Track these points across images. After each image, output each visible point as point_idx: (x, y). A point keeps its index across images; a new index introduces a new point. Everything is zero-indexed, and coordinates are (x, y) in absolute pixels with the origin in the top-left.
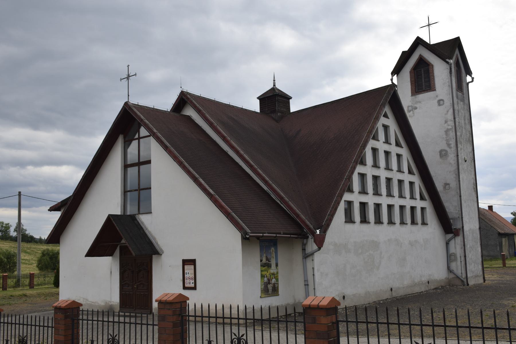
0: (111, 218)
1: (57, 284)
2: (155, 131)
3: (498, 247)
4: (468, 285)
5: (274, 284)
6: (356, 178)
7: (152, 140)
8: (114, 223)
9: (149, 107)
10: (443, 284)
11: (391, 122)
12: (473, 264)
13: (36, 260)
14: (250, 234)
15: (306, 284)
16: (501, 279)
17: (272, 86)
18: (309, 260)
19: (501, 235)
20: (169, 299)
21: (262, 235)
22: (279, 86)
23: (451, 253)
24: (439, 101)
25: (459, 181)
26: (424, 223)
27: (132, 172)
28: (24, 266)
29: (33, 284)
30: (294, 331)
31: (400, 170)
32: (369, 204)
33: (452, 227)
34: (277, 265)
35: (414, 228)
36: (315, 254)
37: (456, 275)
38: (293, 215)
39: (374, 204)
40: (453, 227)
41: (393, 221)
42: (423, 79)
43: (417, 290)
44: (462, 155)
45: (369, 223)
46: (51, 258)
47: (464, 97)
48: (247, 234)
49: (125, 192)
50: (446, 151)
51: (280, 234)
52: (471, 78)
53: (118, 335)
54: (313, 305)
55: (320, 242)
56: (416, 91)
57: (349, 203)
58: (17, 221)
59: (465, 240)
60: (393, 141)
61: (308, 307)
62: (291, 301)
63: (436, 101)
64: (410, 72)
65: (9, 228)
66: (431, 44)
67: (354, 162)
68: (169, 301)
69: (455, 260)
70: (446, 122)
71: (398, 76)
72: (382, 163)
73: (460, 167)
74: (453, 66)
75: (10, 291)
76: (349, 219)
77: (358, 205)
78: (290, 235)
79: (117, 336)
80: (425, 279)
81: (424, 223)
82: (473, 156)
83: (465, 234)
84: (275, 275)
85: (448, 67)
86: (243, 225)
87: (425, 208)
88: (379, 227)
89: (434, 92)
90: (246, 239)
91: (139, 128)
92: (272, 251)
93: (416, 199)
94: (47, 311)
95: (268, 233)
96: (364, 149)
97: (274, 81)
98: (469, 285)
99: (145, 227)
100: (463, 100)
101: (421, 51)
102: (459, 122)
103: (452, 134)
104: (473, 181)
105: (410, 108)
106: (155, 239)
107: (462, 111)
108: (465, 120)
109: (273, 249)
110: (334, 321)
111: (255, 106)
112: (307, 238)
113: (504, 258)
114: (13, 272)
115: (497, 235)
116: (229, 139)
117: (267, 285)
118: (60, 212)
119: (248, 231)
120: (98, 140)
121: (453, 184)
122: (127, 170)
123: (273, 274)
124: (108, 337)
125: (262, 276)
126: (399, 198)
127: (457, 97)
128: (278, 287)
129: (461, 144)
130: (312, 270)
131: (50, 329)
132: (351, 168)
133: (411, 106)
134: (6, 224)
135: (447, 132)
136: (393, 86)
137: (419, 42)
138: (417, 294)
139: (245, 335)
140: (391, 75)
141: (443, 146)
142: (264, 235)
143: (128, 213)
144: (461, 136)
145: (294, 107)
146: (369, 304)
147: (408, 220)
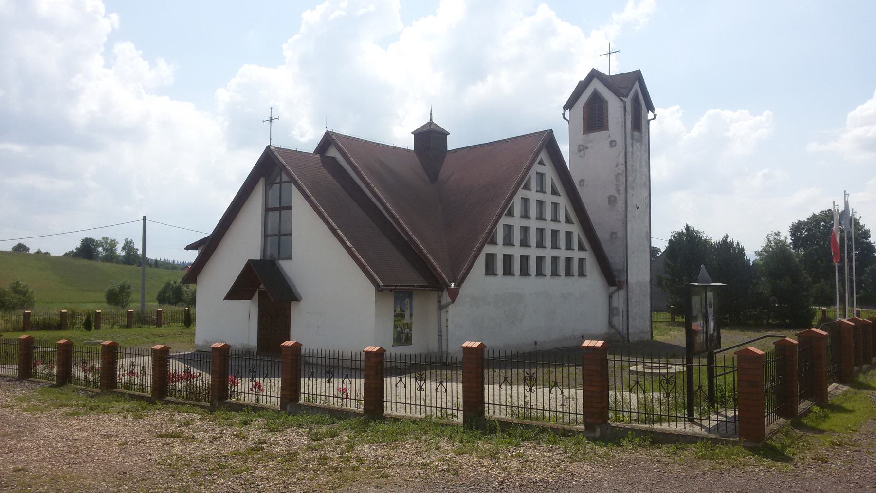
17: (429, 121)
18: (443, 311)
23: (615, 307)
24: (611, 142)
26: (582, 274)
33: (616, 279)
34: (411, 316)
36: (450, 306)
37: (617, 330)
44: (632, 202)
50: (615, 197)
52: (653, 114)
55: (454, 294)
60: (548, 189)
63: (608, 142)
70: (617, 166)
71: (571, 110)
76: (490, 270)
77: (502, 257)
82: (648, 202)
88: (525, 280)
90: (379, 289)
92: (406, 302)
97: (431, 114)
101: (596, 84)
103: (622, 179)
105: (581, 148)
109: (407, 300)
111: (409, 143)
117: (400, 334)
118: (197, 251)
123: (407, 324)
125: (395, 326)
126: (521, 248)
127: (632, 138)
128: (411, 337)
130: (446, 321)
133: (583, 145)
134: (112, 241)
135: (617, 176)
140: (563, 110)
141: (612, 191)
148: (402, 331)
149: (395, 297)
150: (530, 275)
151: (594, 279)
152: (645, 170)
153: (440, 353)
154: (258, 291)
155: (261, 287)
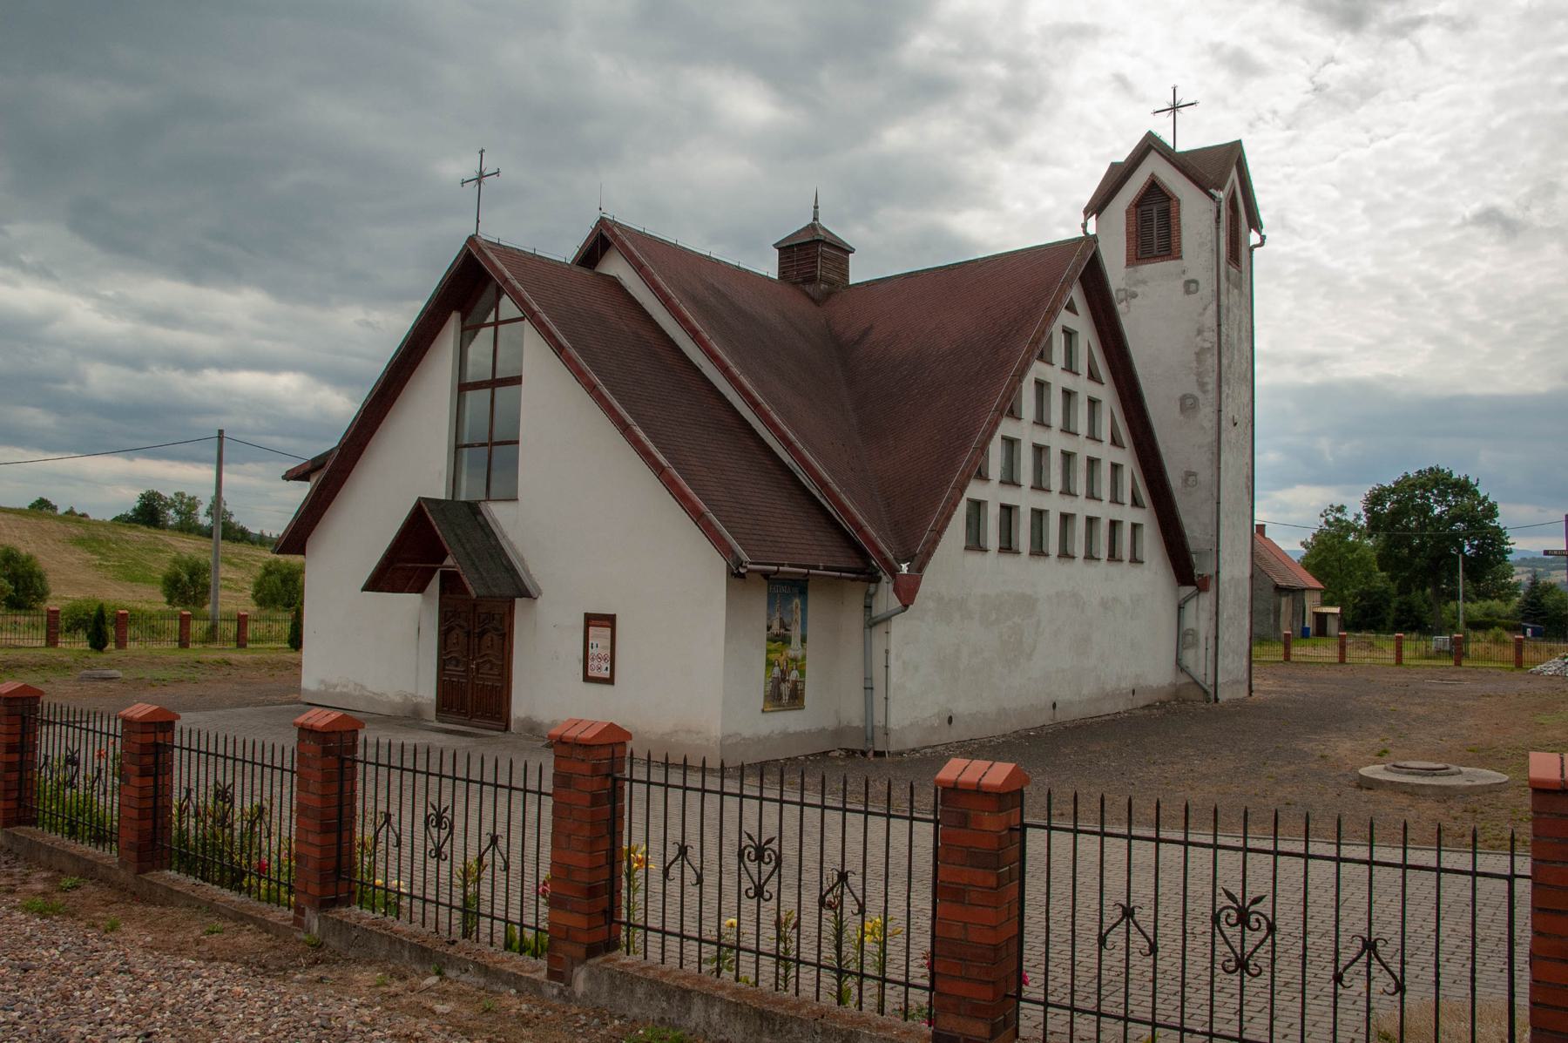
0: (424, 505)
1: (296, 641)
2: (536, 307)
3: (1272, 616)
4: (1216, 700)
5: (795, 683)
6: (996, 450)
7: (528, 328)
8: (431, 518)
9: (524, 252)
10: (1163, 697)
11: (1081, 323)
12: (1231, 656)
13: (249, 582)
14: (749, 566)
15: (869, 685)
16: (1284, 689)
17: (810, 220)
18: (878, 632)
19: (1279, 590)
20: (582, 736)
21: (776, 568)
22: (827, 223)
24: (1188, 283)
25: (1219, 468)
26: (1135, 560)
27: (477, 401)
28: (226, 593)
29: (245, 638)
30: (841, 795)
31: (1093, 436)
32: (1021, 509)
34: (804, 640)
35: (1114, 569)
36: (893, 618)
38: (847, 526)
39: (1033, 510)
40: (1197, 572)
41: (1069, 552)
42: (1155, 229)
43: (1108, 708)
44: (1229, 411)
45: (1018, 553)
46: (284, 581)
47: (1241, 278)
48: (741, 565)
49: (458, 447)
50: (1195, 399)
51: (816, 568)
53: (1270, 897)
54: (965, 783)
55: (907, 594)
56: (1136, 255)
57: (977, 506)
58: (213, 493)
59: (1220, 602)
60: (1082, 366)
61: (952, 786)
62: (830, 723)
63: (1180, 284)
64: (1128, 212)
65: (195, 507)
66: (1179, 149)
67: (996, 410)
68: (583, 740)
69: (1195, 644)
70: (1200, 332)
72: (1056, 416)
73: (1223, 436)
74: (1223, 205)
75: (195, 651)
76: (975, 543)
78: (841, 572)
79: (449, 811)
80: (1126, 685)
81: (1135, 560)
83: (1221, 587)
84: (799, 664)
85: (1213, 206)
86: (734, 543)
87: (1141, 525)
88: (1040, 565)
89: (1178, 261)
90: (736, 575)
91: (499, 298)
93: (1123, 504)
94: (274, 704)
95: (790, 565)
96: (1021, 381)
97: (816, 207)
98: (1220, 702)
99: (501, 532)
100: (1238, 286)
101: (1154, 165)
102: (1228, 336)
103: (1211, 361)
104: (1247, 470)
106: (522, 560)
107: (1236, 311)
108: (1240, 331)
109: (797, 601)
110: (1015, 822)
111: (768, 266)
112: (878, 580)
113: (1287, 643)
114: (203, 605)
115: (1272, 590)
116: (706, 336)
119: (744, 557)
120: (399, 322)
121: (1205, 475)
122: (465, 396)
123: (794, 660)
124: (426, 812)
125: (770, 664)
127: (1228, 278)
128: (803, 690)
129: (1228, 384)
130: (884, 655)
131: (287, 775)
132: (989, 423)
134: (190, 499)
135: (1200, 354)
136: (1089, 241)
137: (1150, 145)
138: (1107, 718)
139: (776, 841)
142: (781, 568)
143: (463, 498)
144: (1230, 366)
145: (859, 273)
146: (1004, 736)
147: (1103, 550)
148: (783, 678)
149: (769, 593)
150: (1047, 555)
151: (1154, 572)
152: (1246, 346)
153: (869, 729)
154: (438, 573)
155: (445, 563)
